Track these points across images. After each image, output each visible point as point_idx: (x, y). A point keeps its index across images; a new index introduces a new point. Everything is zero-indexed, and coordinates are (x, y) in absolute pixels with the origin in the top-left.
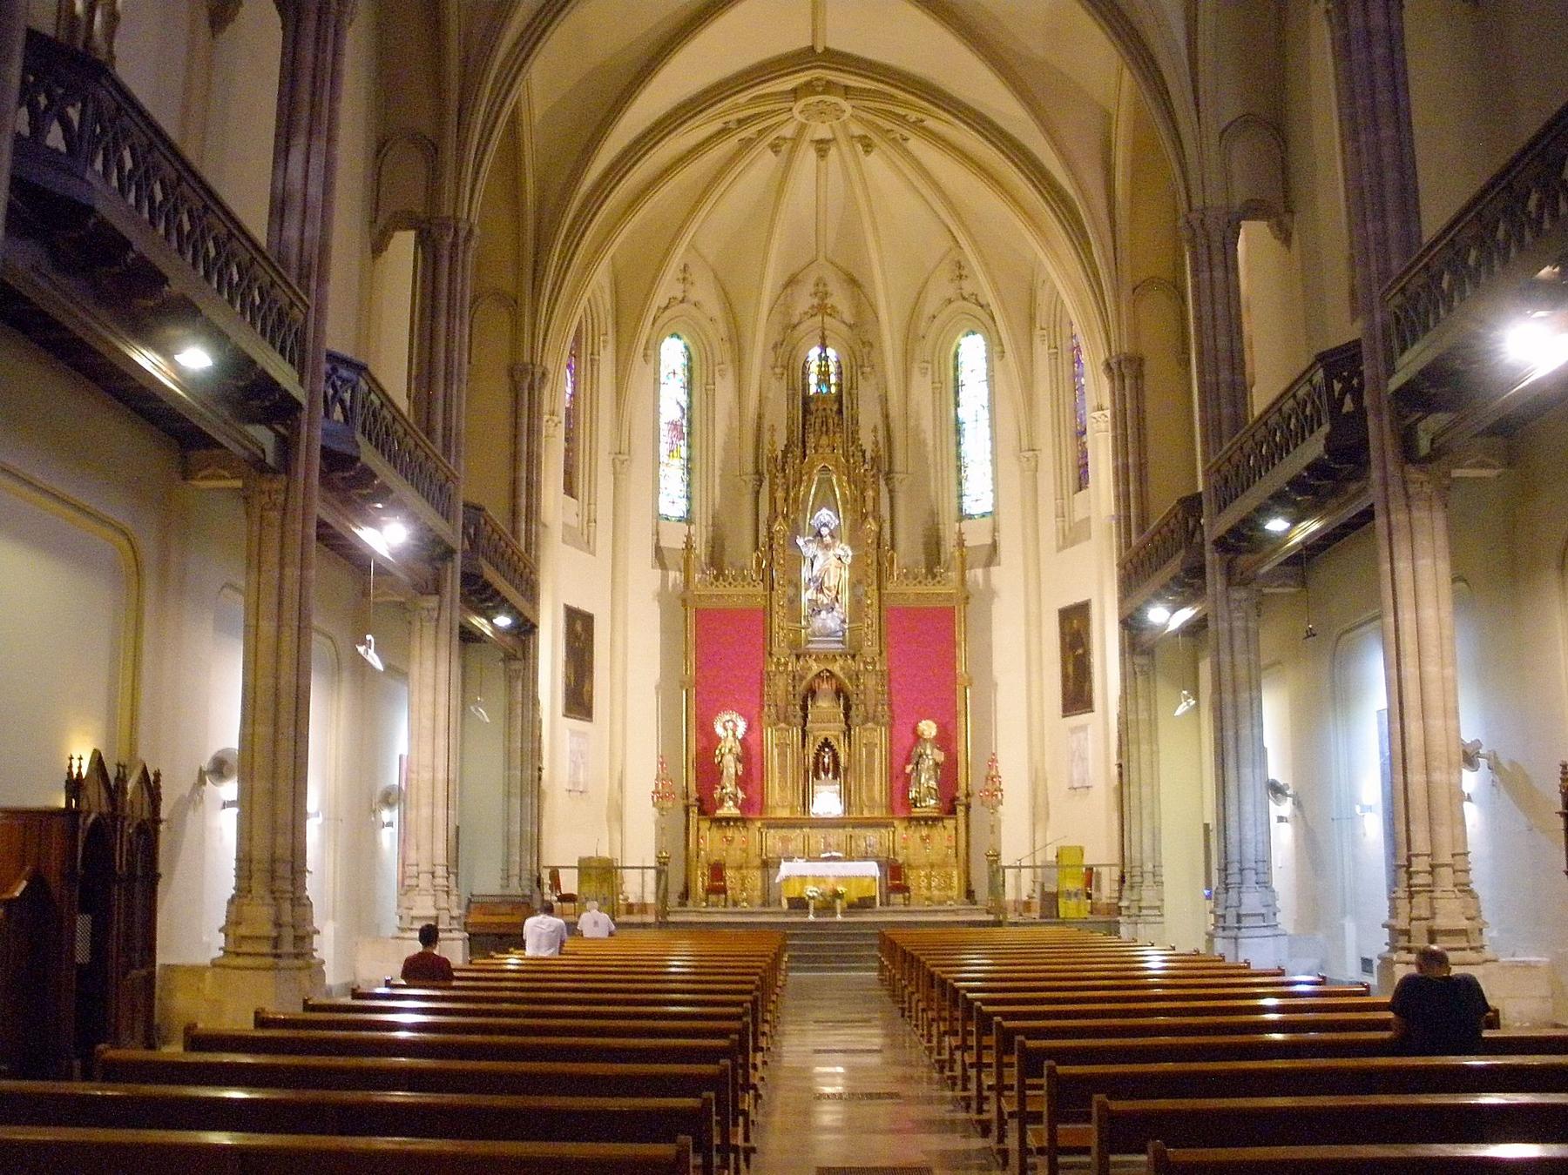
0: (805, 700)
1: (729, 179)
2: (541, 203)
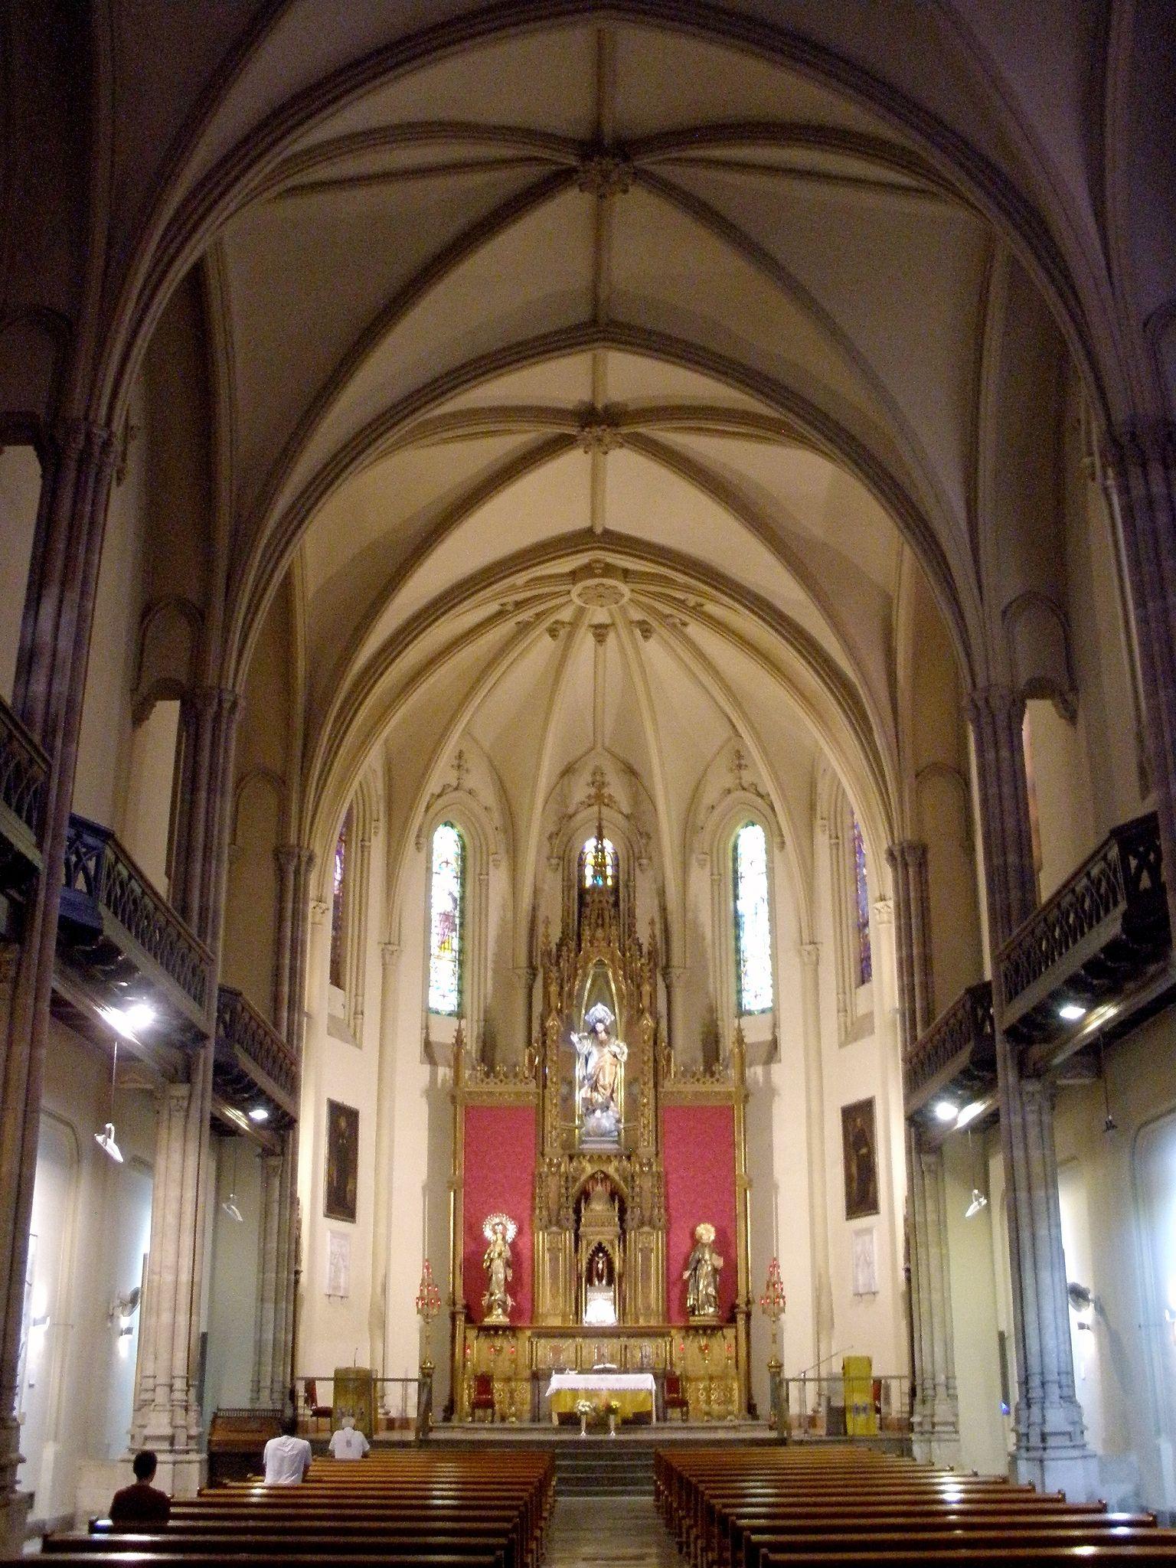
0: (578, 1203)
1: (506, 663)
2: (311, 676)
